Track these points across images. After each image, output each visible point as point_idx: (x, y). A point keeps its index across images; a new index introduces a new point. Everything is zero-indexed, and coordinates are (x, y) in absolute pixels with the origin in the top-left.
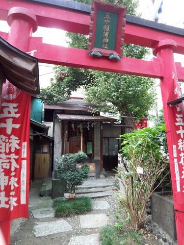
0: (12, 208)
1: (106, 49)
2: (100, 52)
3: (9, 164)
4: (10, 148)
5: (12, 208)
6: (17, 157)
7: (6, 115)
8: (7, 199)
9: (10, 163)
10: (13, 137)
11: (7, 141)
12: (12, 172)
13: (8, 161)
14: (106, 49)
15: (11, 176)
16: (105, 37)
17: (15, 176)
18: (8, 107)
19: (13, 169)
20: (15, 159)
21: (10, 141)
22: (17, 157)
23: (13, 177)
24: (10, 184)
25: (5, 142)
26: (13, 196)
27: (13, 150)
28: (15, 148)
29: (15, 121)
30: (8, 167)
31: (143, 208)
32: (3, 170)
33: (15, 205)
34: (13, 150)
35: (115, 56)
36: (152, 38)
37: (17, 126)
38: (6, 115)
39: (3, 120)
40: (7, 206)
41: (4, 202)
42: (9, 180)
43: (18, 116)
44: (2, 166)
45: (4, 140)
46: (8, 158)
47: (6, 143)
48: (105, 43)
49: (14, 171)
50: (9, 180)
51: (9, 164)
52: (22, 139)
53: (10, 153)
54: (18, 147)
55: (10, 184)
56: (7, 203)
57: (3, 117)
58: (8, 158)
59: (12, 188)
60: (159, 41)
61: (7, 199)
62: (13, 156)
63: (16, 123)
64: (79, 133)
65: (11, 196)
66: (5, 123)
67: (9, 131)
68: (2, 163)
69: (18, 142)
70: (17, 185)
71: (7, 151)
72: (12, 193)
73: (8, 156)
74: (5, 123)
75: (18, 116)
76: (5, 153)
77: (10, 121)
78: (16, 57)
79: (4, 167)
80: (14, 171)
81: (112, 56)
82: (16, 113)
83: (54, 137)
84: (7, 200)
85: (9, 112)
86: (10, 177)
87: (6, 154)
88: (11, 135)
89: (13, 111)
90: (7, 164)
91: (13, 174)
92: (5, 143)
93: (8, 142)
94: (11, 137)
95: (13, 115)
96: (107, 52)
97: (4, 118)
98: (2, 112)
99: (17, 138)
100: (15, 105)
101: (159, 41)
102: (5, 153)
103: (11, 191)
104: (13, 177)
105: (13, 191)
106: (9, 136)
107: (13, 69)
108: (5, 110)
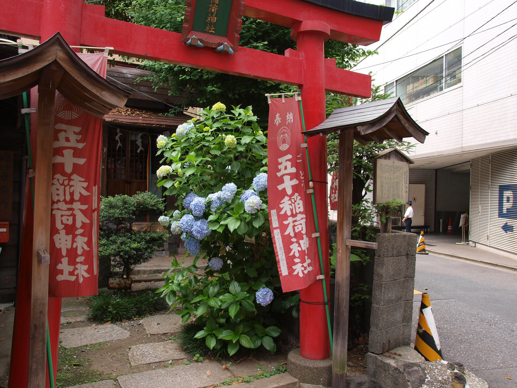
0: (81, 280)
1: (212, 33)
2: (201, 41)
3: (72, 217)
4: (72, 194)
5: (81, 280)
6: (84, 207)
7: (62, 143)
8: (71, 268)
9: (74, 216)
10: (75, 177)
11: (66, 183)
12: (77, 229)
13: (70, 213)
14: (212, 33)
15: (77, 235)
16: (212, 13)
17: (82, 235)
18: (65, 131)
19: (79, 224)
20: (81, 210)
21: (71, 183)
22: (84, 207)
23: (79, 237)
24: (74, 246)
25: (63, 184)
26: (81, 263)
27: (77, 197)
28: (80, 193)
29: (77, 153)
30: (70, 222)
31: (88, 111)
32: (63, 226)
33: (87, 275)
34: (77, 197)
35: (226, 49)
36: (290, 16)
37: (82, 161)
38: (62, 143)
39: (59, 151)
40: (73, 278)
41: (68, 273)
42: (73, 241)
43: (81, 146)
44: (62, 220)
45: (61, 182)
46: (69, 209)
47: (65, 186)
48: (211, 23)
49: (81, 228)
50: (73, 241)
51: (72, 217)
52: (92, 181)
53: (72, 201)
54: (85, 193)
55: (74, 246)
56: (71, 273)
57: (58, 146)
58: (69, 209)
59: (80, 251)
60: (301, 22)
61: (71, 268)
62: (77, 206)
63: (80, 157)
64: (79, 77)
65: (78, 263)
66: (62, 155)
67: (68, 169)
68: (62, 216)
69: (85, 185)
70: (86, 248)
71: (68, 198)
72: (80, 259)
73: (69, 206)
74: (62, 155)
75: (81, 146)
76: (65, 200)
77: (68, 153)
78: (105, 90)
79: (64, 222)
80: (81, 228)
81: (222, 47)
82: (78, 141)
83: (299, 318)
84: (71, 270)
85: (67, 140)
86: (75, 236)
87: (66, 203)
88: (72, 174)
89: (73, 138)
90: (68, 217)
91: (80, 231)
92: (63, 187)
93: (68, 184)
94: (72, 177)
95: (73, 143)
96: (213, 40)
97: (60, 147)
98: (57, 139)
99: (83, 180)
100: (78, 129)
101: (301, 22)
102: (65, 200)
103: (77, 256)
104: (79, 237)
105: (82, 255)
106: (69, 177)
107: (86, 92)
108: (62, 136)
